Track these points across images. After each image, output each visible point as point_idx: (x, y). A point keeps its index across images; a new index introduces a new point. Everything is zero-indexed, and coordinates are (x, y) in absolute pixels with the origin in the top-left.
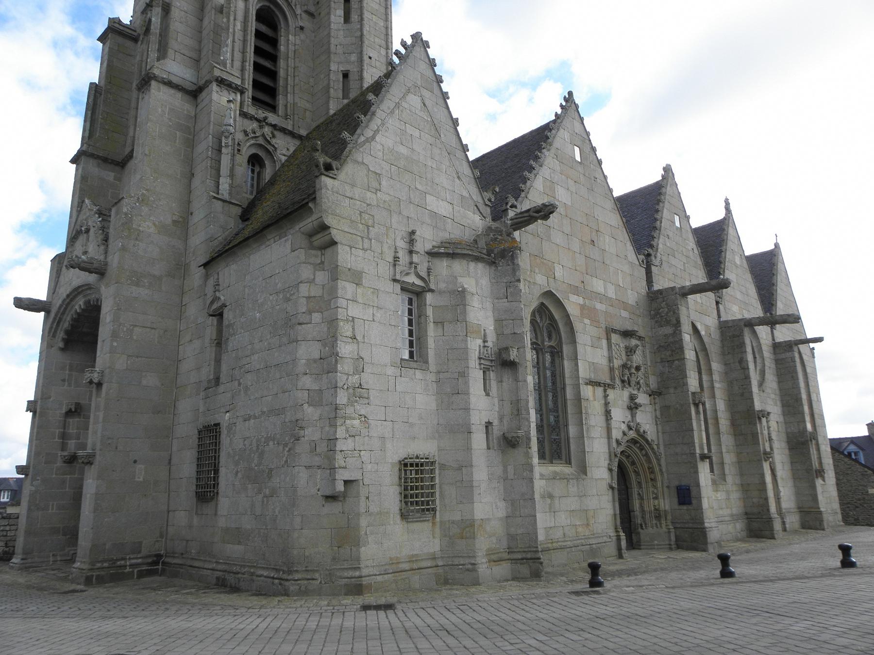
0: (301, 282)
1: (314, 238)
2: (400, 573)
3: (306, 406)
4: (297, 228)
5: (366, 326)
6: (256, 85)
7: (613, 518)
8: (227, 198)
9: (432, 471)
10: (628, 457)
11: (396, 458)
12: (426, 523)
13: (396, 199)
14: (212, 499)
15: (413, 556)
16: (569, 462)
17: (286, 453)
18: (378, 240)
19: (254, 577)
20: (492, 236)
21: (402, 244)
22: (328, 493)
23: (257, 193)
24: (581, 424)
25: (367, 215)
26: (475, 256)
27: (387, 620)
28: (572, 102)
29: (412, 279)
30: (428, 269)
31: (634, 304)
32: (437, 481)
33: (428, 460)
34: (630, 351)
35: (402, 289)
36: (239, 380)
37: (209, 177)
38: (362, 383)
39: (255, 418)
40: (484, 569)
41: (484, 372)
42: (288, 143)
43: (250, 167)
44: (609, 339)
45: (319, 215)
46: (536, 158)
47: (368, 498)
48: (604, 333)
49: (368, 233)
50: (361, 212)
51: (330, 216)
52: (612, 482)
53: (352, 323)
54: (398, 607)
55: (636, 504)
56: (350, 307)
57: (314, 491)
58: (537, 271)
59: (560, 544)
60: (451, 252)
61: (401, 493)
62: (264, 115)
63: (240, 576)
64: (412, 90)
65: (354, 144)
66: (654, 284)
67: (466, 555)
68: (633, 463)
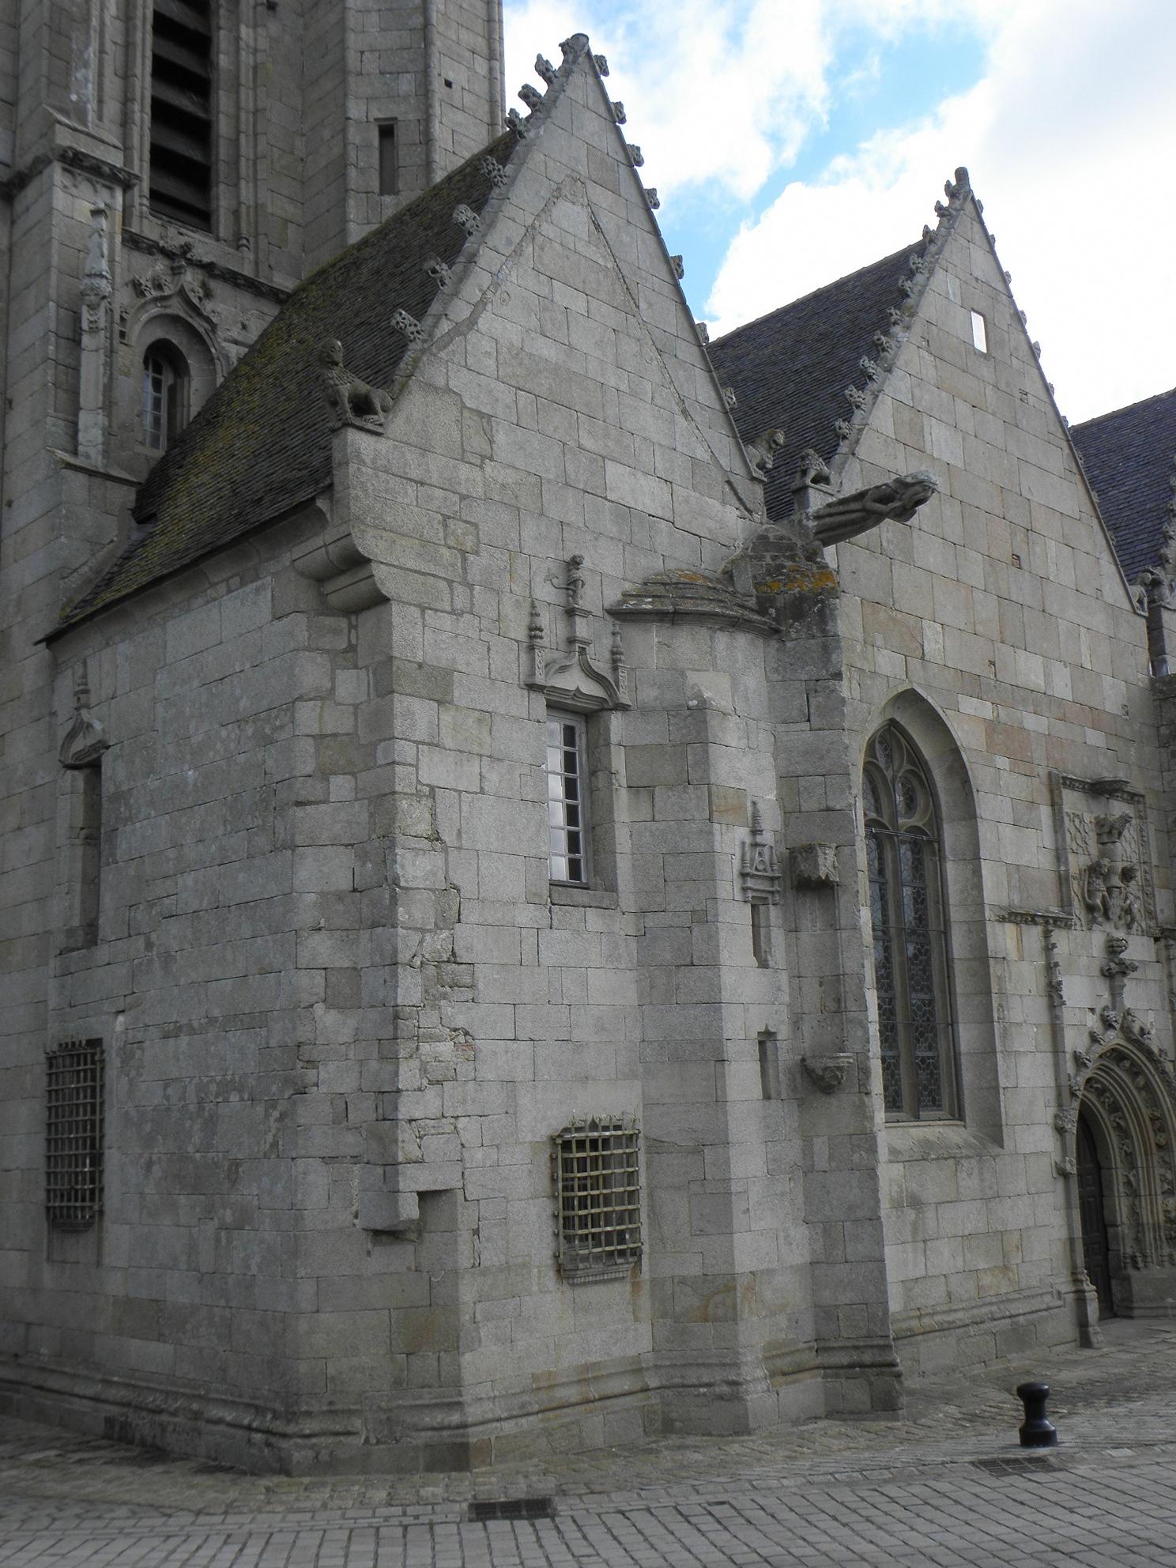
0: (300, 698)
1: (330, 587)
2: (558, 1412)
3: (319, 1009)
4: (286, 559)
5: (465, 808)
6: (161, 158)
7: (1068, 1248)
8: (99, 464)
9: (630, 1159)
10: (1102, 1092)
11: (544, 1131)
12: (616, 1285)
13: (532, 479)
14: (88, 1225)
15: (587, 1367)
16: (958, 1114)
17: (274, 1125)
18: (488, 586)
19: (202, 1424)
20: (769, 560)
21: (547, 593)
22: (380, 1225)
23: (171, 448)
24: (987, 1019)
25: (462, 525)
26: (730, 617)
27: (539, 1553)
28: (965, 199)
29: (574, 681)
30: (613, 653)
31: (1119, 712)
32: (643, 1180)
33: (619, 1133)
34: (1108, 832)
35: (551, 706)
36: (147, 936)
37: (51, 411)
38: (456, 949)
39: (192, 1031)
40: (759, 1395)
41: (753, 906)
42: (244, 311)
43: (151, 373)
44: (1055, 805)
45: (343, 530)
46: (877, 351)
47: (476, 1232)
48: (1045, 791)
49: (464, 569)
50: (446, 517)
51: (371, 532)
52: (1064, 1161)
53: (430, 802)
54: (562, 1506)
55: (1122, 1209)
56: (424, 760)
57: (344, 1217)
58: (879, 641)
59: (938, 1318)
60: (671, 608)
61: (556, 1217)
62: (182, 240)
63: (164, 1418)
64: (565, 191)
65: (425, 341)
66: (1168, 657)
67: (715, 1361)
68: (1114, 1108)
